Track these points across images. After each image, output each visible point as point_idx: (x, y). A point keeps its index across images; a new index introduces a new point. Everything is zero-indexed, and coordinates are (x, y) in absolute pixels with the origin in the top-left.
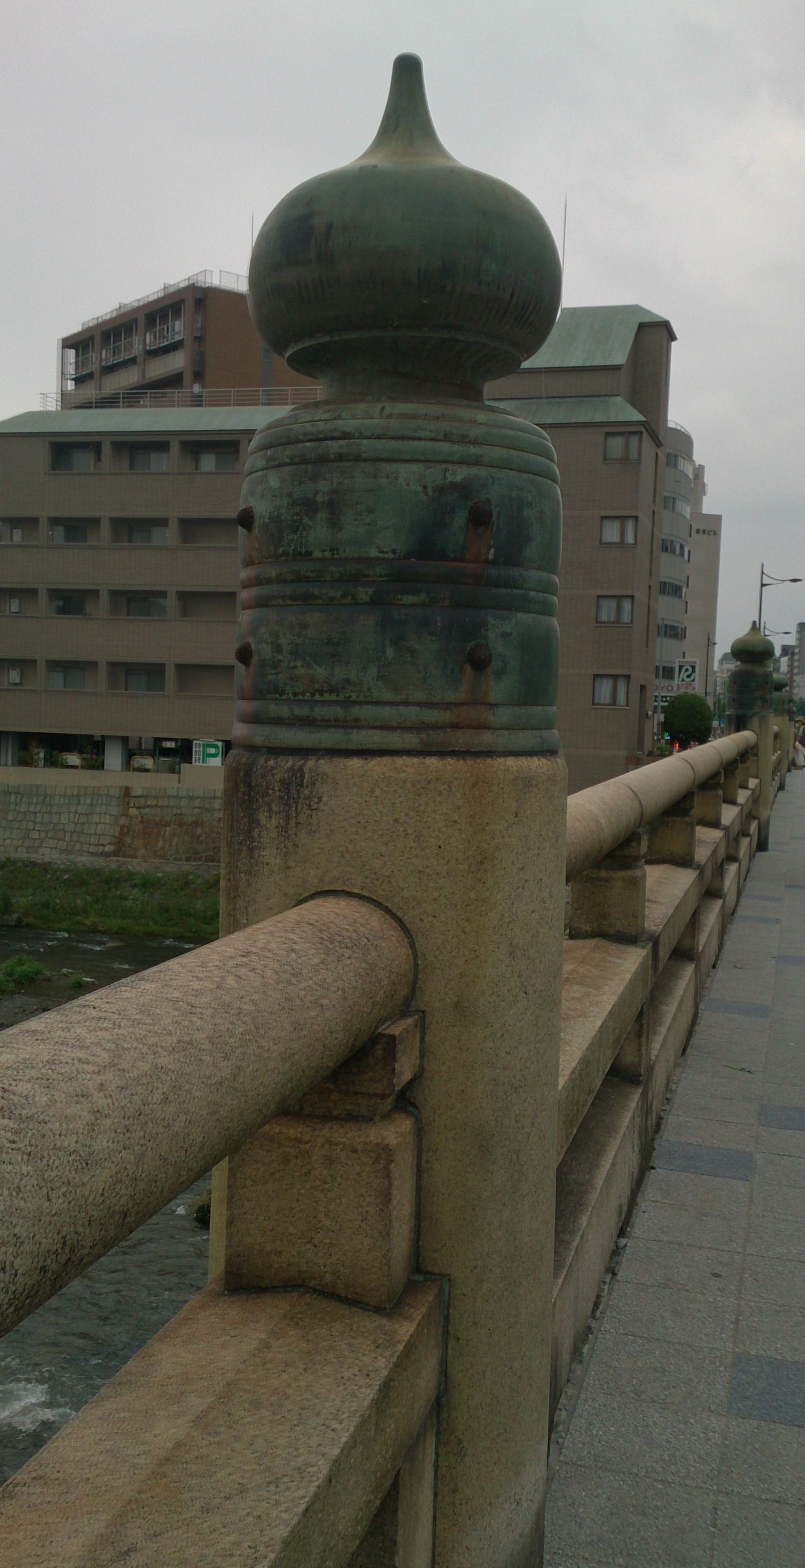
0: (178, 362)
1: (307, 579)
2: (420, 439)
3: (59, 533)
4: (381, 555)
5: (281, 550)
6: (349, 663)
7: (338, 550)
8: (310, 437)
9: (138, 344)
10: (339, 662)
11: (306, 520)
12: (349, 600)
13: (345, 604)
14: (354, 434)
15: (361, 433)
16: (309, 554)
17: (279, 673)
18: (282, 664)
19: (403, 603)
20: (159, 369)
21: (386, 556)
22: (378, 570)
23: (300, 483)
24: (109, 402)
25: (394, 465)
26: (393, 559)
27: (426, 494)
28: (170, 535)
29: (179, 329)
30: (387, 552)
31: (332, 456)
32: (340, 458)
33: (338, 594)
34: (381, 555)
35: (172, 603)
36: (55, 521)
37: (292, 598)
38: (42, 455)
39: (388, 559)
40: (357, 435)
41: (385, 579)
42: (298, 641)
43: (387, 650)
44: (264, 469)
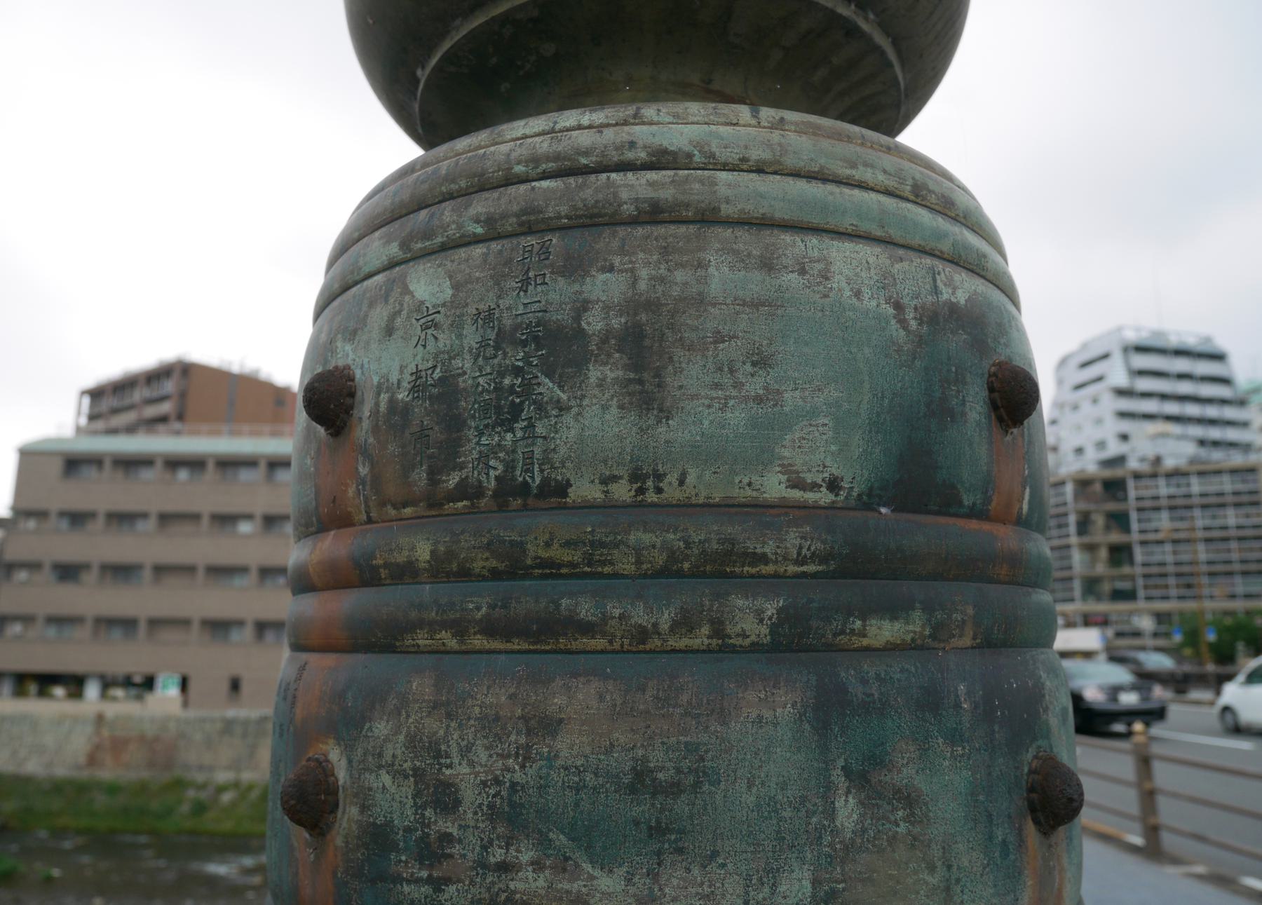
0: (166, 408)
1: (550, 569)
2: (862, 186)
3: (64, 524)
4: (796, 494)
5: (453, 480)
6: (715, 854)
7: (659, 477)
8: (551, 166)
9: (138, 395)
10: (680, 851)
11: (547, 387)
12: (702, 637)
13: (688, 651)
14: (690, 156)
15: (713, 155)
16: (556, 491)
17: (448, 881)
18: (456, 850)
19: (865, 642)
20: (151, 411)
21: (810, 496)
22: (792, 540)
23: (525, 284)
24: (113, 431)
25: (813, 241)
26: (832, 507)
27: (903, 323)
28: (150, 525)
29: (169, 386)
30: (814, 486)
31: (628, 209)
32: (654, 214)
33: (665, 619)
34: (796, 494)
35: (147, 574)
36: (62, 514)
37: (490, 629)
38: (57, 466)
39: (816, 507)
40: (698, 158)
41: (811, 568)
42: (518, 776)
43: (840, 803)
44: (391, 265)
